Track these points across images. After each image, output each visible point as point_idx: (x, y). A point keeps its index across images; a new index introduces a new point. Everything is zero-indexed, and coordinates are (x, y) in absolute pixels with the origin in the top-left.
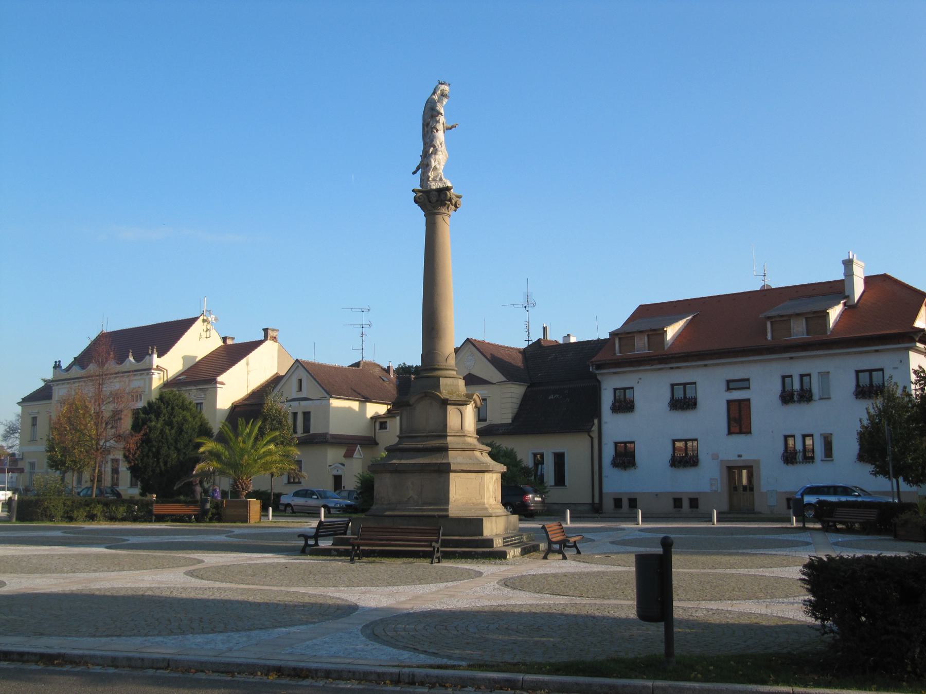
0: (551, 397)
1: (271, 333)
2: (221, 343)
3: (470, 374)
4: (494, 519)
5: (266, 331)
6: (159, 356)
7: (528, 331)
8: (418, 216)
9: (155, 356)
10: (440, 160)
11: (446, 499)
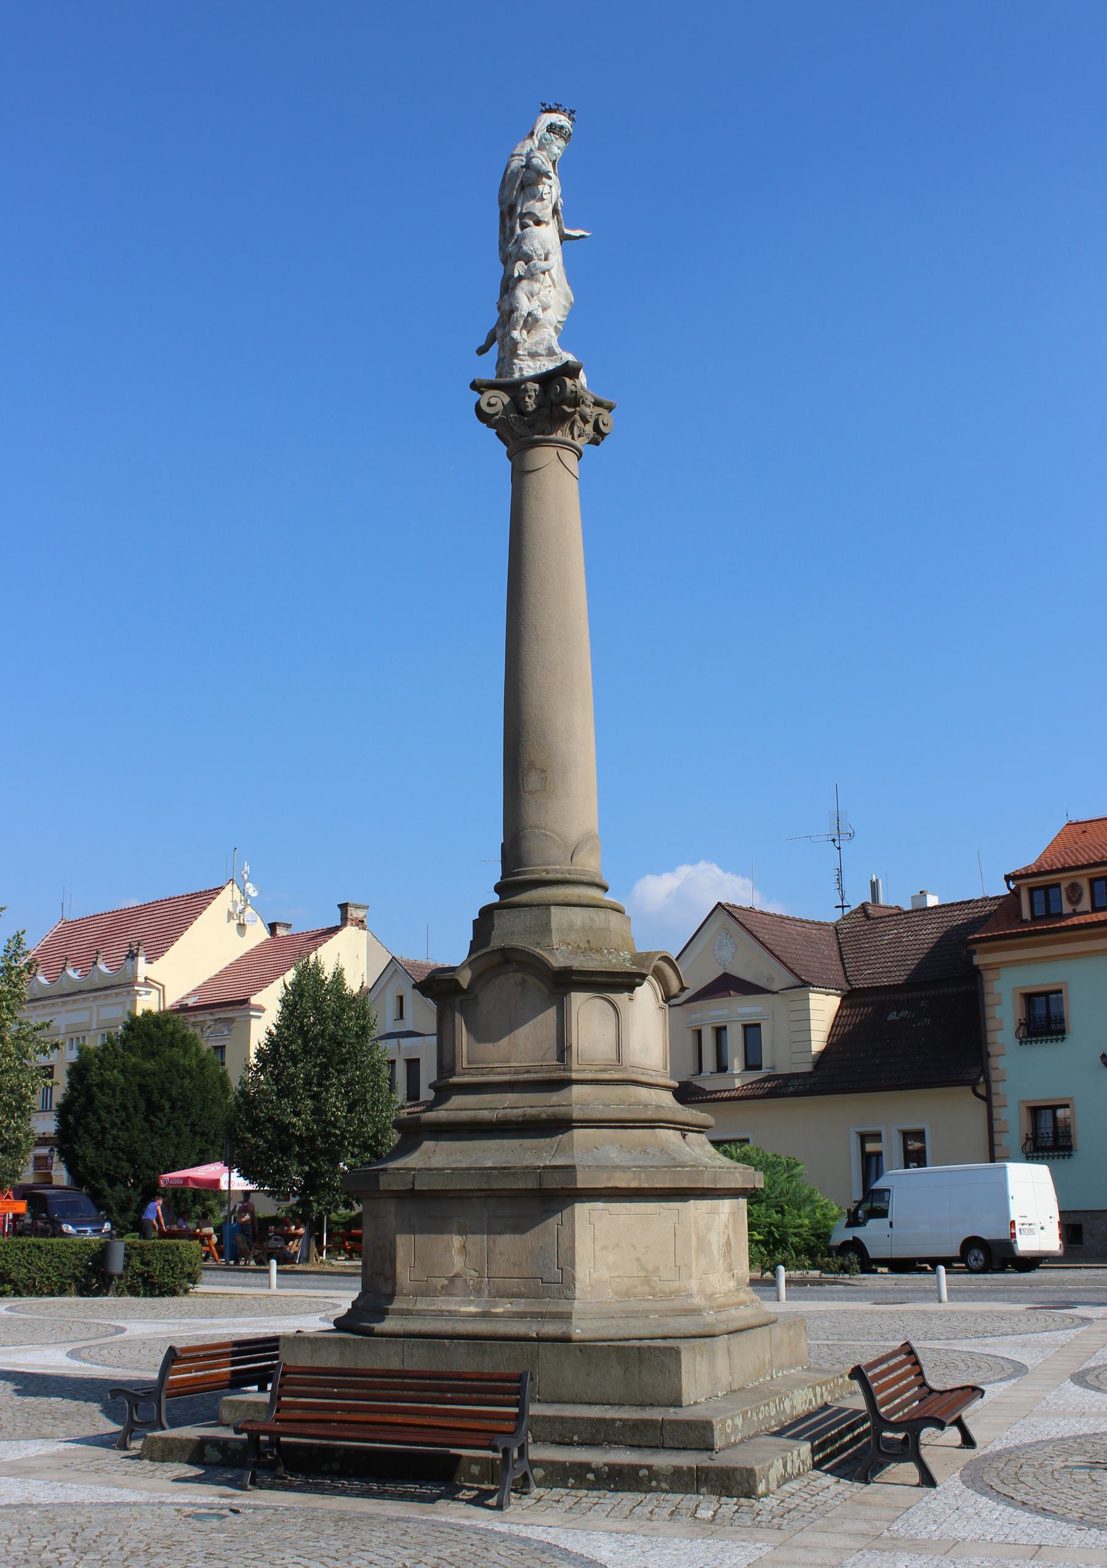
0: (893, 1016)
1: (353, 913)
2: (265, 935)
3: (725, 975)
4: (721, 1342)
5: (344, 907)
6: (149, 961)
7: (840, 888)
8: (493, 450)
9: (141, 960)
10: (548, 297)
11: (565, 1284)
